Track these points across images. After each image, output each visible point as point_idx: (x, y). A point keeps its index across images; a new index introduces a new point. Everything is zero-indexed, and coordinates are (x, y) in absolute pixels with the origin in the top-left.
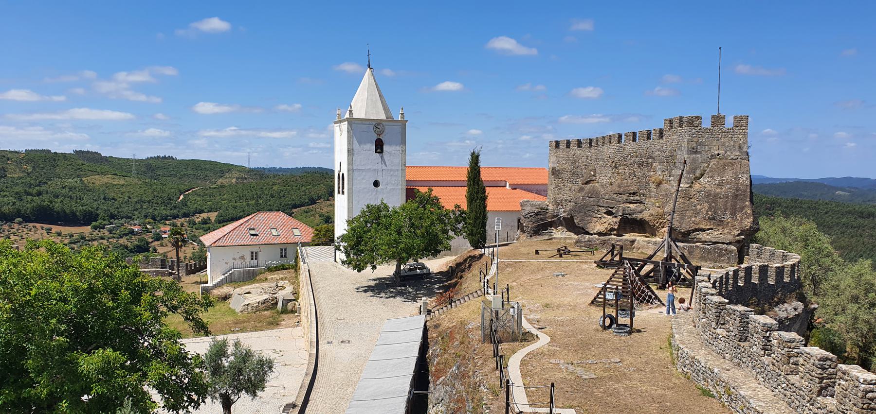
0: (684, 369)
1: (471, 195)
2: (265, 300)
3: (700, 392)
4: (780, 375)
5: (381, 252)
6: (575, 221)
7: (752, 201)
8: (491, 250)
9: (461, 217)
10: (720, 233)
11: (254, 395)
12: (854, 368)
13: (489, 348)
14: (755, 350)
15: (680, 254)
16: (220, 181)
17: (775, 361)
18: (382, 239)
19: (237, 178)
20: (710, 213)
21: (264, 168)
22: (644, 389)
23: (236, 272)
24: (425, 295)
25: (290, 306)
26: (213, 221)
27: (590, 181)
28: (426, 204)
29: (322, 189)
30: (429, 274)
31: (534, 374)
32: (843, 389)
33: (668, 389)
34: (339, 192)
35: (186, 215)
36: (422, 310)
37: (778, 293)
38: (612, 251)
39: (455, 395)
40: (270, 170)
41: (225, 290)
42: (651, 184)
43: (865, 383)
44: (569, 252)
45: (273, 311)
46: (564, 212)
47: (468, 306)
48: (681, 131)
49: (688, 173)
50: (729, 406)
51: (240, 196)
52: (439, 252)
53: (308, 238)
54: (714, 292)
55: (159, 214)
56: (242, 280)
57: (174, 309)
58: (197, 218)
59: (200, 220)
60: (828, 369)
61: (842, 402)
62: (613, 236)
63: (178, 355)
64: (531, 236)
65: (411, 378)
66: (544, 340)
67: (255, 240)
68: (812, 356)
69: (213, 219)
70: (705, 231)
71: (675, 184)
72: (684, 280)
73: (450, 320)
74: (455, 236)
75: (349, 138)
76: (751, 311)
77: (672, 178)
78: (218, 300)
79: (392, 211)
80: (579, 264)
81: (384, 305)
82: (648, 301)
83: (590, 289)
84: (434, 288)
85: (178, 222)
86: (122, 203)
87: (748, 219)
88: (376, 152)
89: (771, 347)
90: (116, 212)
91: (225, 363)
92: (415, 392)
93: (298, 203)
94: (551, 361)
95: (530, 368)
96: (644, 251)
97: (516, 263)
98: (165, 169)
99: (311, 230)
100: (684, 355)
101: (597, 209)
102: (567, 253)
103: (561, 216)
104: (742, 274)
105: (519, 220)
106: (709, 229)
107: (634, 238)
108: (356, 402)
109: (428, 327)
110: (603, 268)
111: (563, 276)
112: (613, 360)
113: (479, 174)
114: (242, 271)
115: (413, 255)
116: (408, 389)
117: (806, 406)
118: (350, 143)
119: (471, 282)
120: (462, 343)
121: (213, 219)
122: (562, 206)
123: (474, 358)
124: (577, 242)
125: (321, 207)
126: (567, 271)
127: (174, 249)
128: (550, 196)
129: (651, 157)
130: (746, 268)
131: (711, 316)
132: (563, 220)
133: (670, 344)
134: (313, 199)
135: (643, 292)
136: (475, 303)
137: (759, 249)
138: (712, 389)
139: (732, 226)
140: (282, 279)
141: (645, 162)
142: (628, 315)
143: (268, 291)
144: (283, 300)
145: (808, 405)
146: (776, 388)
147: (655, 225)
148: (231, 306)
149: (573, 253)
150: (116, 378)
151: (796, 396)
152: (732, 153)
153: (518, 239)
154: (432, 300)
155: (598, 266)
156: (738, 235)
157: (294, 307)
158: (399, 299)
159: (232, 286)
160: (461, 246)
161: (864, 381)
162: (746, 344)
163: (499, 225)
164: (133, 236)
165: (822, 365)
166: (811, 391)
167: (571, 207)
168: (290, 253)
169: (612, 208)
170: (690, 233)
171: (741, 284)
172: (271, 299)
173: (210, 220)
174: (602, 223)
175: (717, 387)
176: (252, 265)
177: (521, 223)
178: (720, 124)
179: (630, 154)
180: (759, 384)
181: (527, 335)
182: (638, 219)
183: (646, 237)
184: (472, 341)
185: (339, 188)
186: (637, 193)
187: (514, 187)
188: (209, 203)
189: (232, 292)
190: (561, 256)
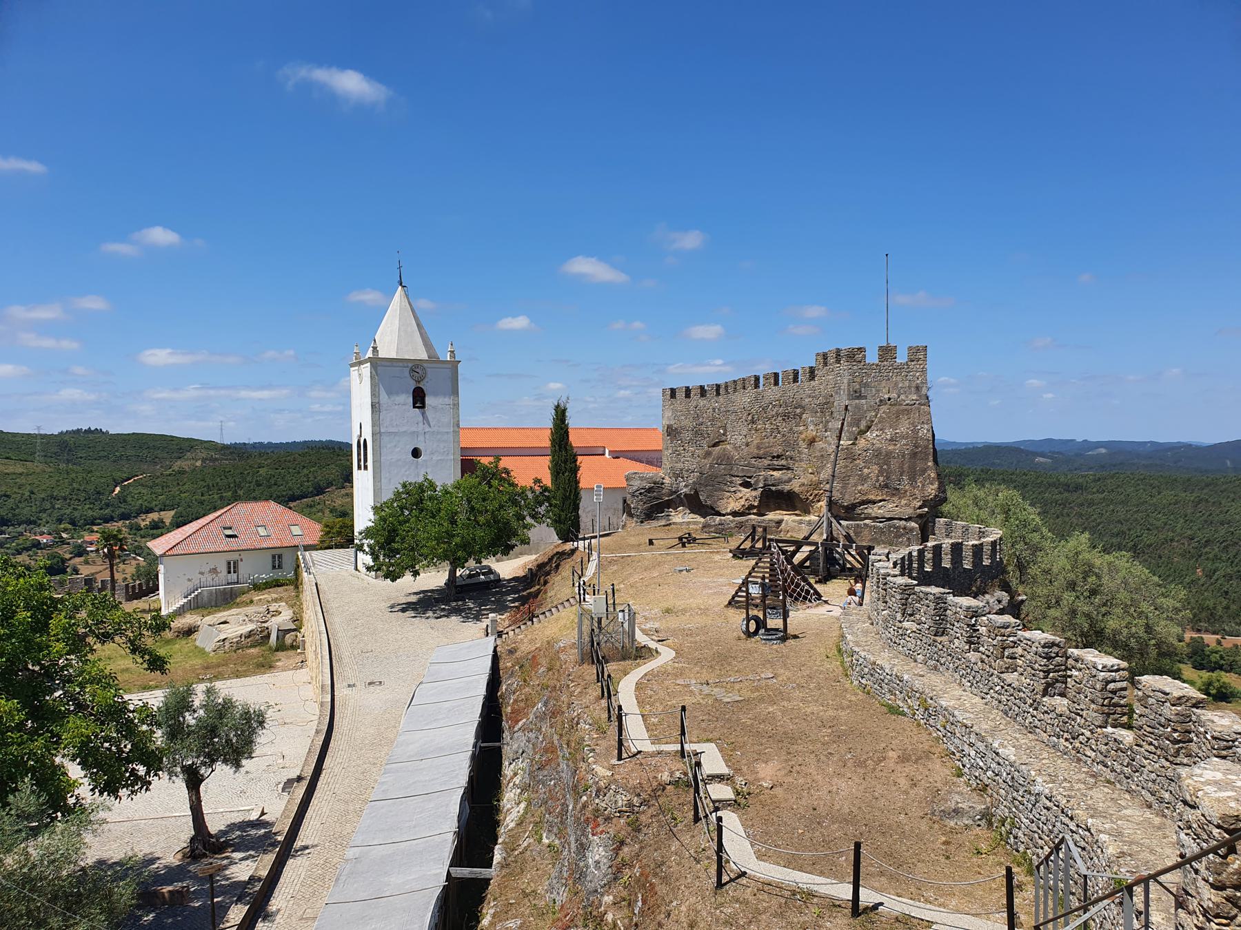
0: (862, 681)
1: (556, 465)
2: (251, 631)
3: (885, 709)
4: (992, 675)
5: (425, 551)
6: (701, 497)
7: (935, 461)
8: (587, 542)
9: (544, 496)
11: (238, 765)
12: (1089, 653)
13: (590, 671)
14: (957, 644)
15: (845, 534)
16: (177, 465)
17: (984, 657)
18: (426, 530)
19: (204, 460)
20: (881, 479)
21: (245, 444)
22: (809, 710)
23: (205, 593)
24: (493, 611)
25: (289, 639)
26: (168, 524)
28: (491, 479)
29: (333, 472)
30: (498, 581)
31: (655, 701)
32: (1076, 681)
33: (843, 708)
34: (359, 468)
35: (124, 517)
36: (489, 631)
37: (976, 580)
39: (542, 742)
40: (254, 445)
41: (189, 619)
42: (801, 443)
43: (1105, 670)
44: (695, 539)
45: (263, 648)
46: (686, 486)
47: (557, 620)
49: (850, 425)
50: (926, 724)
51: (208, 485)
52: (512, 547)
53: (314, 538)
55: (81, 516)
56: (213, 604)
57: (105, 637)
58: (143, 520)
59: (148, 523)
60: (1054, 658)
61: (1075, 700)
62: (753, 516)
63: (112, 706)
64: (642, 522)
65: (476, 725)
66: (666, 655)
68: (1033, 643)
69: (168, 521)
70: (875, 503)
71: (834, 441)
72: (852, 569)
73: (532, 641)
74: (535, 524)
76: (949, 593)
78: (178, 636)
79: (441, 491)
81: (432, 628)
82: (805, 598)
83: (725, 586)
84: (506, 601)
85: (113, 527)
86: (20, 502)
87: (932, 484)
88: (414, 407)
89: (979, 638)
90: (10, 515)
91: (190, 719)
92: (483, 745)
93: (298, 493)
94: (678, 682)
95: (650, 692)
97: (623, 557)
98: (89, 448)
99: (318, 527)
100: (861, 660)
104: (928, 555)
105: (625, 501)
106: (881, 501)
107: (780, 517)
108: (394, 765)
109: (499, 654)
110: (741, 558)
111: (688, 571)
112: (763, 676)
113: (568, 436)
114: (214, 591)
115: (475, 554)
116: (472, 740)
117: (1028, 713)
118: (374, 394)
119: (560, 586)
120: (550, 669)
121: (168, 521)
123: (568, 685)
124: (704, 527)
125: (334, 498)
126: (694, 565)
127: (106, 569)
129: (800, 406)
130: (934, 546)
131: (895, 605)
133: (839, 651)
134: (320, 487)
135: (798, 585)
136: (568, 615)
138: (901, 705)
140: (275, 600)
141: (793, 413)
143: (255, 619)
144: (278, 630)
145: (1031, 710)
146: (987, 694)
147: (808, 499)
148: (197, 643)
149: (700, 541)
150: (8, 745)
151: (1014, 700)
152: (907, 397)
153: (624, 527)
154: (503, 617)
156: (920, 508)
157: (295, 640)
158: (454, 619)
159: (198, 613)
160: (544, 538)
161: (1103, 667)
162: (944, 639)
163: (600, 495)
164: (39, 551)
165: (1047, 654)
166: (1034, 690)
167: (695, 480)
168: (287, 562)
170: (856, 507)
171: (928, 569)
172: (259, 630)
173: (163, 522)
174: (736, 499)
175: (909, 701)
176: (230, 581)
177: (628, 505)
180: (964, 691)
181: (643, 650)
183: (797, 515)
184: (565, 663)
185: (359, 460)
187: (616, 455)
188: (160, 497)
189: (199, 623)
190: (684, 546)
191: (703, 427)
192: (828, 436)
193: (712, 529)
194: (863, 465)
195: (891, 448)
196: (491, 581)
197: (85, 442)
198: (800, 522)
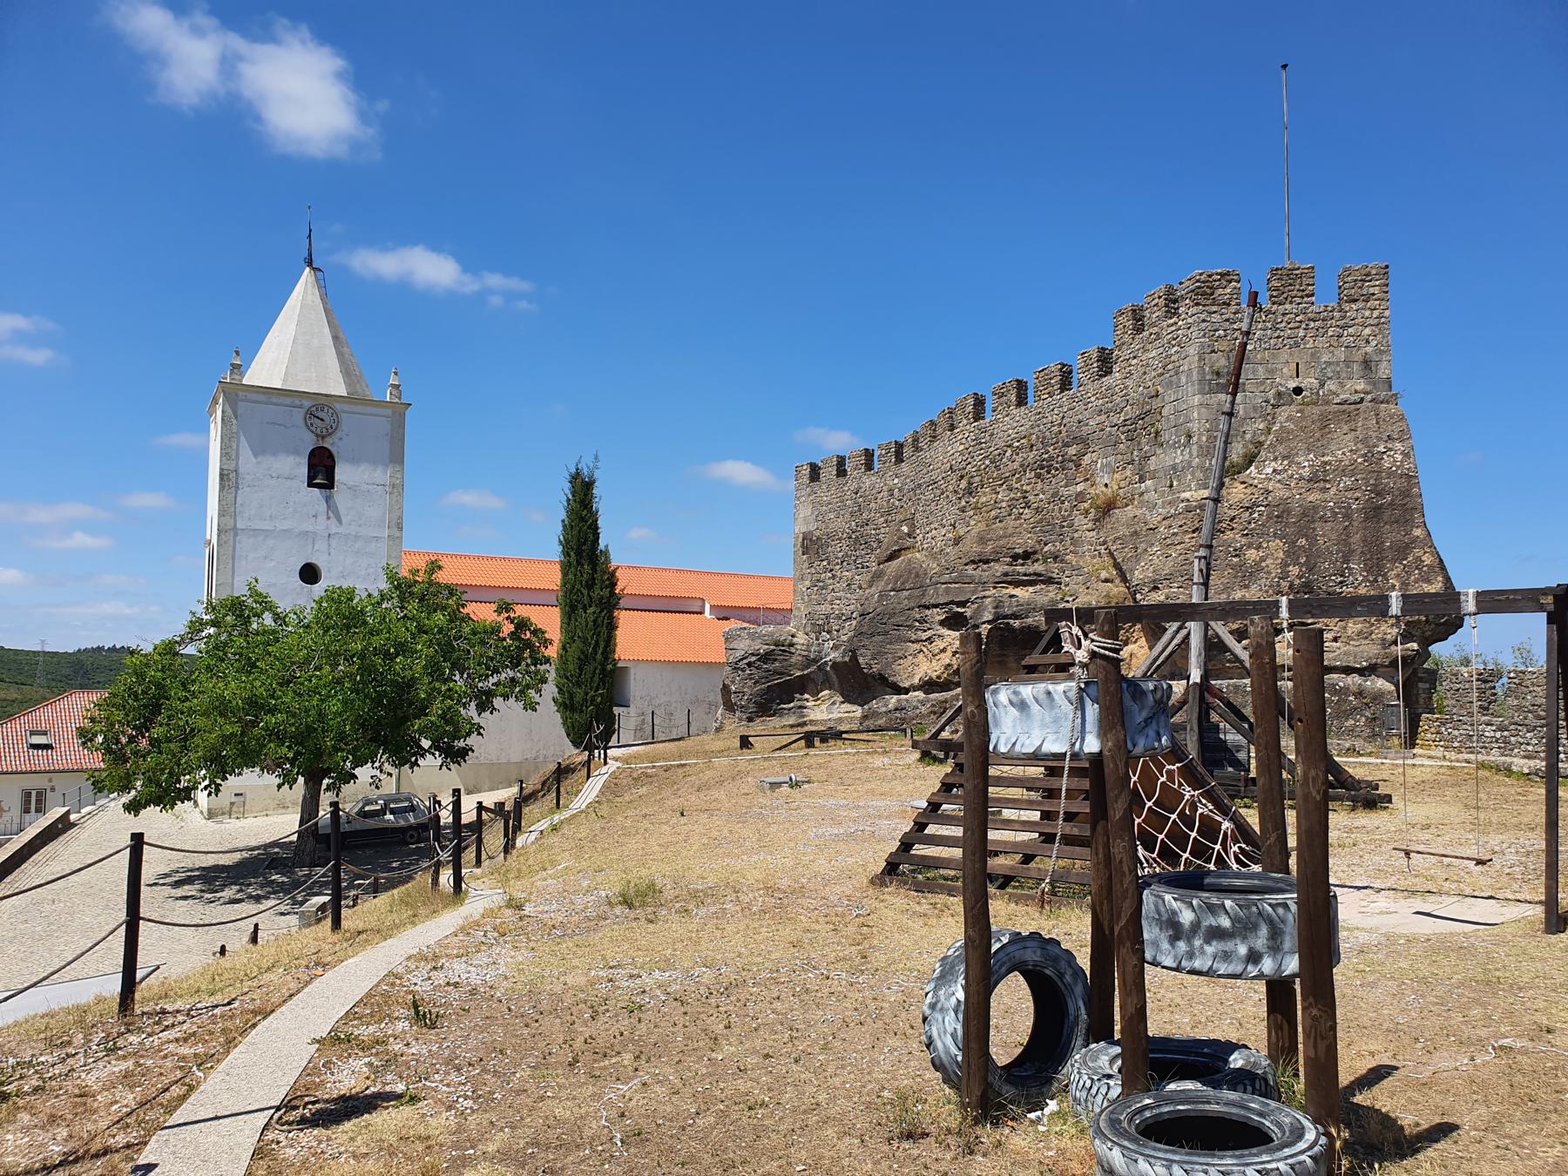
6: (861, 660)
20: (1294, 570)
27: (899, 550)
46: (835, 647)
48: (1173, 328)
64: (750, 720)
67: (41, 760)
75: (226, 440)
88: (310, 485)
101: (918, 616)
103: (828, 659)
111: (794, 785)
122: (829, 632)
132: (832, 673)
135: (1170, 799)
137: (1485, 682)
142: (1275, 934)
152: (1342, 385)
169: (963, 604)
178: (1300, 294)
179: (1009, 446)
186: (1035, 553)
191: (869, 530)
192: (1147, 491)
194: (1244, 541)
196: (410, 827)
197: (107, 664)
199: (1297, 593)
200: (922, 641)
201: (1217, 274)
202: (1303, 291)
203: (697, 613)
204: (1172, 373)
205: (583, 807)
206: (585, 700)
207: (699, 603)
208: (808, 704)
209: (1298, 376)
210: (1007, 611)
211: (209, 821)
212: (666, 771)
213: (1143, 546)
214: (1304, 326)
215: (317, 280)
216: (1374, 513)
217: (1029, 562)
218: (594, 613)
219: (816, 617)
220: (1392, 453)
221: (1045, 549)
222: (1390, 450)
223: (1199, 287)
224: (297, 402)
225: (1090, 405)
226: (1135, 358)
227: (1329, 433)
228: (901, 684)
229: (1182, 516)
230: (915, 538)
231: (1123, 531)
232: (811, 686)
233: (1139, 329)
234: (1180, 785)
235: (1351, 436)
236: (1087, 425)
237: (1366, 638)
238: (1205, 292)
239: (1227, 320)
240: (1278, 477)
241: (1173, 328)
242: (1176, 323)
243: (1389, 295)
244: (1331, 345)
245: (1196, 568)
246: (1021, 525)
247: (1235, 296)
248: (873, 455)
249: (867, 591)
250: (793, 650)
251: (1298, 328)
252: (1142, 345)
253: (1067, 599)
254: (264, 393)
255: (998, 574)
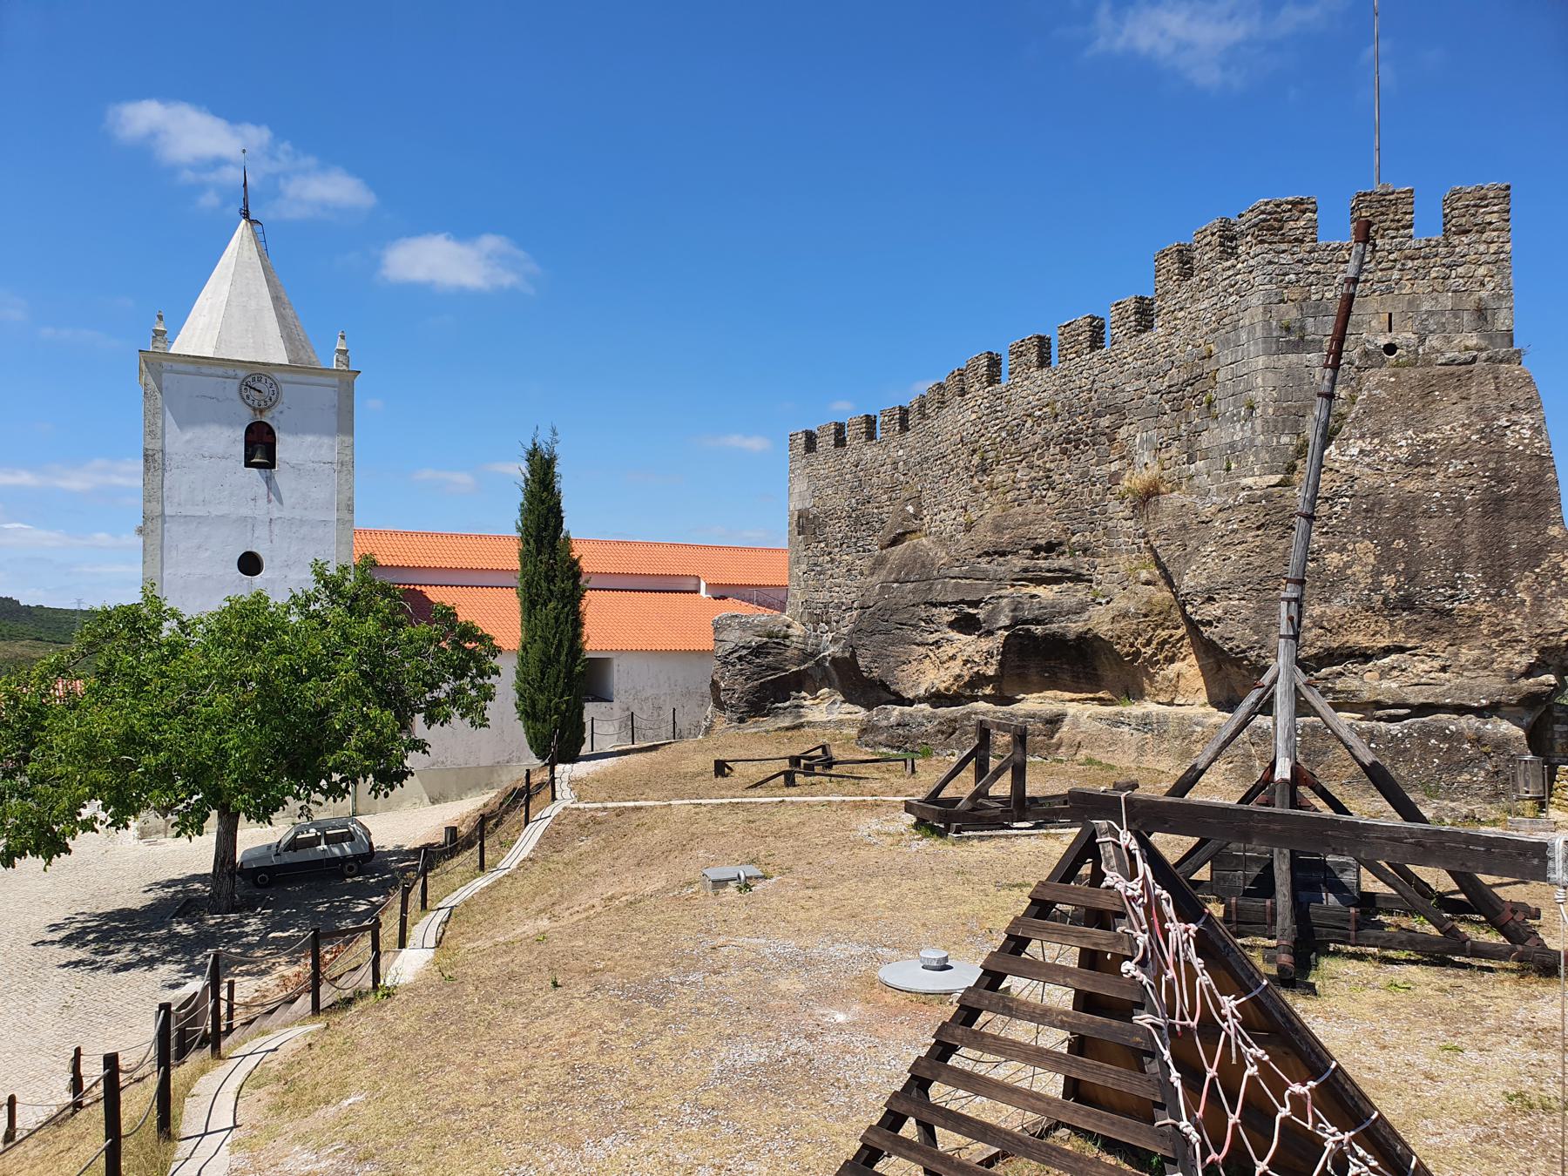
6: (860, 662)
10: (1437, 664)
20: (1389, 580)
27: (904, 534)
38: (980, 755)
42: (1113, 506)
46: (835, 641)
48: (1230, 273)
54: (1515, 967)
62: (982, 705)
64: (741, 720)
77: (1200, 464)
80: (847, 815)
88: (248, 464)
96: (1099, 755)
97: (620, 812)
101: (923, 615)
102: (818, 769)
103: (826, 653)
106: (1387, 651)
107: (1056, 708)
110: (942, 834)
111: (745, 886)
122: (827, 623)
124: (863, 731)
128: (795, 595)
139: (1497, 634)
147: (1137, 654)
152: (1448, 340)
155: (920, 824)
156: (1529, 672)
169: (975, 604)
178: (1394, 225)
179: (1029, 416)
182: (1071, 636)
183: (1102, 701)
186: (1060, 544)
187: (721, 592)
191: (871, 508)
192: (1198, 474)
193: (882, 738)
195: (1413, 485)
196: (344, 859)
198: (1116, 722)
199: (1393, 609)
200: (927, 644)
201: (1287, 203)
202: (1399, 221)
203: (692, 592)
204: (1228, 328)
205: (514, 866)
206: (548, 708)
207: (694, 581)
208: (805, 703)
209: (1390, 331)
210: (1027, 615)
211: (141, 842)
212: (618, 815)
213: (1194, 543)
214: (1399, 266)
215: (255, 234)
216: (1495, 505)
217: (1054, 555)
218: (555, 609)
219: (813, 605)
220: (1518, 427)
221: (1073, 540)
222: (1515, 423)
223: (1265, 220)
224: (231, 372)
225: (1126, 367)
226: (1181, 309)
227: (1433, 402)
228: (904, 695)
229: (1243, 508)
230: (921, 519)
231: (1167, 523)
232: (808, 683)
233: (1187, 274)
234: (1317, 1120)
235: (1460, 407)
236: (1123, 391)
237: (1486, 668)
238: (1271, 226)
239: (1300, 261)
240: (1367, 460)
241: (1230, 273)
242: (1234, 266)
243: (1510, 225)
244: (1434, 290)
245: (1284, 615)
246: (1044, 510)
247: (1310, 231)
248: (875, 422)
249: (869, 580)
250: (788, 643)
251: (1391, 268)
252: (1190, 294)
253: (1099, 600)
254: (192, 363)
255: (1017, 570)
